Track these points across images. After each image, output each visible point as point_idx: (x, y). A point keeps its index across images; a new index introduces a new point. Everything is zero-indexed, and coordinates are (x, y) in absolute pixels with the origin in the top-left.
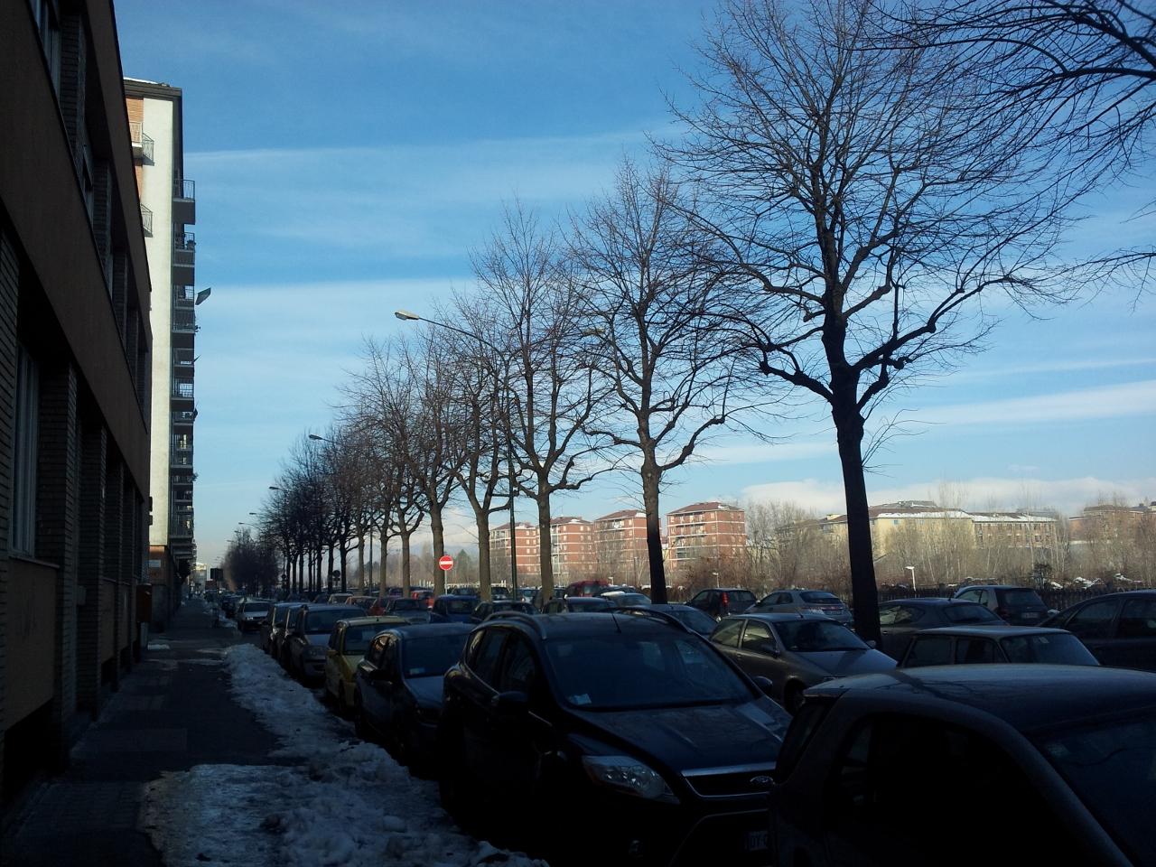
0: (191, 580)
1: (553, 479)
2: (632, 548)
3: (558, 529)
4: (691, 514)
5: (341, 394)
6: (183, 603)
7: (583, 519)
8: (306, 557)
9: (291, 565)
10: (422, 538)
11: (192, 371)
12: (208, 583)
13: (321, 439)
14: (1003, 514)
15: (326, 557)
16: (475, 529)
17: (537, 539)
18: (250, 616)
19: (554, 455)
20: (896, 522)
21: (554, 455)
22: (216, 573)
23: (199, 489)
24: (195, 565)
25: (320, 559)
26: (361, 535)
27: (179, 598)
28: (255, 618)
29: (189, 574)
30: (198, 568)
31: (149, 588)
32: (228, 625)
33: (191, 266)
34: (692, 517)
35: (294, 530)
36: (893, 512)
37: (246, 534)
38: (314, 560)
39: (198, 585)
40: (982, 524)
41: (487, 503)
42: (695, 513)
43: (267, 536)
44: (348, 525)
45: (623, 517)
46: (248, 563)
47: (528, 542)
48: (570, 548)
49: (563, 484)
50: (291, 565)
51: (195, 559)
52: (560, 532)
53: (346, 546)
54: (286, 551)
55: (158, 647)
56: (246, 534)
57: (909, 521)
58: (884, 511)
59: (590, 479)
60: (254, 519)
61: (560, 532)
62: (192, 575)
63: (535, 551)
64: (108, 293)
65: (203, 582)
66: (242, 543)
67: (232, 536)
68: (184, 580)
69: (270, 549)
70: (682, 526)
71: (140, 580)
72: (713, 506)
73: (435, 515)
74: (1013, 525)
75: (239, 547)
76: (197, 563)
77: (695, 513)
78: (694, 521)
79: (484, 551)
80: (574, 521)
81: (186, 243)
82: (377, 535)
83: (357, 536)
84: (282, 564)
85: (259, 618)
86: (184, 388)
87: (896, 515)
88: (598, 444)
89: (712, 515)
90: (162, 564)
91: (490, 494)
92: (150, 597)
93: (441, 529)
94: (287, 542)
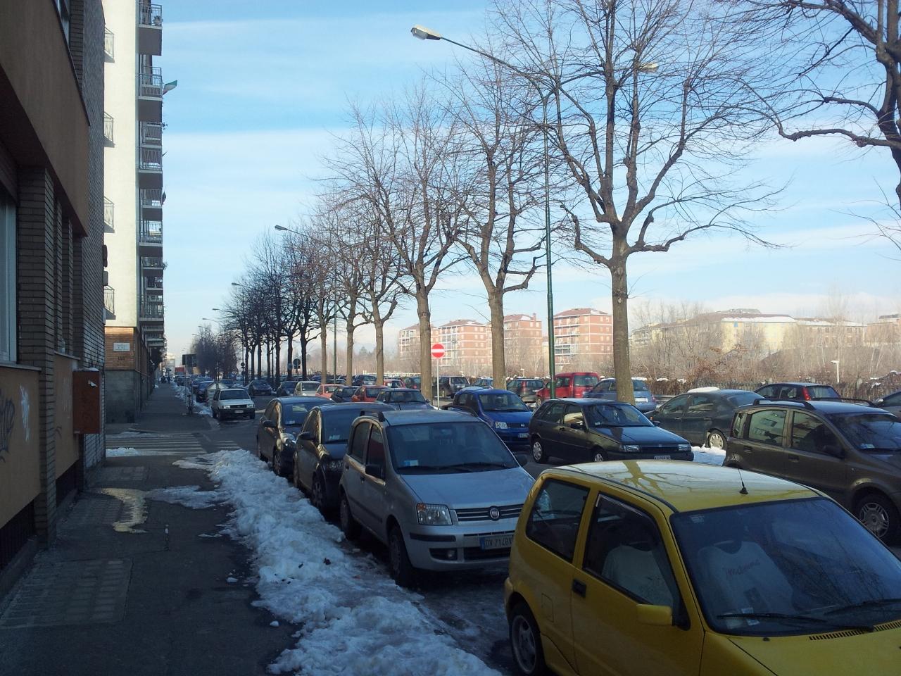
0: (163, 367)
1: (632, 237)
2: (588, 342)
3: (456, 329)
4: (568, 318)
5: (262, 248)
6: (157, 386)
7: (477, 321)
8: (264, 347)
9: (250, 354)
10: (365, 336)
11: (162, 291)
12: (176, 369)
13: (286, 230)
14: (821, 320)
15: (284, 347)
16: (487, 311)
17: (434, 334)
18: (227, 404)
19: (633, 208)
20: (736, 325)
21: (633, 208)
22: (186, 359)
23: (169, 280)
24: (166, 355)
25: (278, 349)
26: (323, 326)
27: (152, 381)
28: (231, 406)
29: (162, 361)
30: (168, 357)
31: (95, 376)
32: (202, 413)
33: (159, 99)
34: (568, 320)
35: (251, 322)
36: (733, 316)
37: (208, 329)
38: (272, 349)
39: (168, 370)
40: (813, 328)
41: (501, 280)
42: (572, 317)
43: (228, 327)
44: (308, 317)
45: (511, 320)
46: (210, 356)
47: (476, 337)
48: (466, 345)
49: (641, 246)
50: (250, 354)
51: (166, 350)
52: (459, 332)
53: (306, 336)
54: (245, 342)
55: (122, 452)
56: (208, 329)
57: (749, 324)
58: (727, 316)
59: (681, 238)
60: (217, 314)
61: (459, 332)
62: (164, 363)
63: (608, 338)
64: (65, 40)
65: (173, 369)
66: (204, 336)
67: (197, 331)
68: (157, 366)
69: (230, 341)
70: (560, 328)
71: (81, 363)
72: (586, 311)
73: (422, 299)
74: (830, 329)
75: (202, 340)
76: (168, 353)
77: (572, 317)
78: (571, 323)
79: (498, 337)
80: (470, 323)
81: (153, 19)
82: (342, 325)
83: (320, 326)
84: (241, 353)
85: (236, 406)
86: (153, 228)
87: (736, 319)
88: (684, 195)
89: (586, 318)
90: (132, 347)
91: (504, 270)
92: (97, 390)
93: (428, 315)
94: (245, 333)
